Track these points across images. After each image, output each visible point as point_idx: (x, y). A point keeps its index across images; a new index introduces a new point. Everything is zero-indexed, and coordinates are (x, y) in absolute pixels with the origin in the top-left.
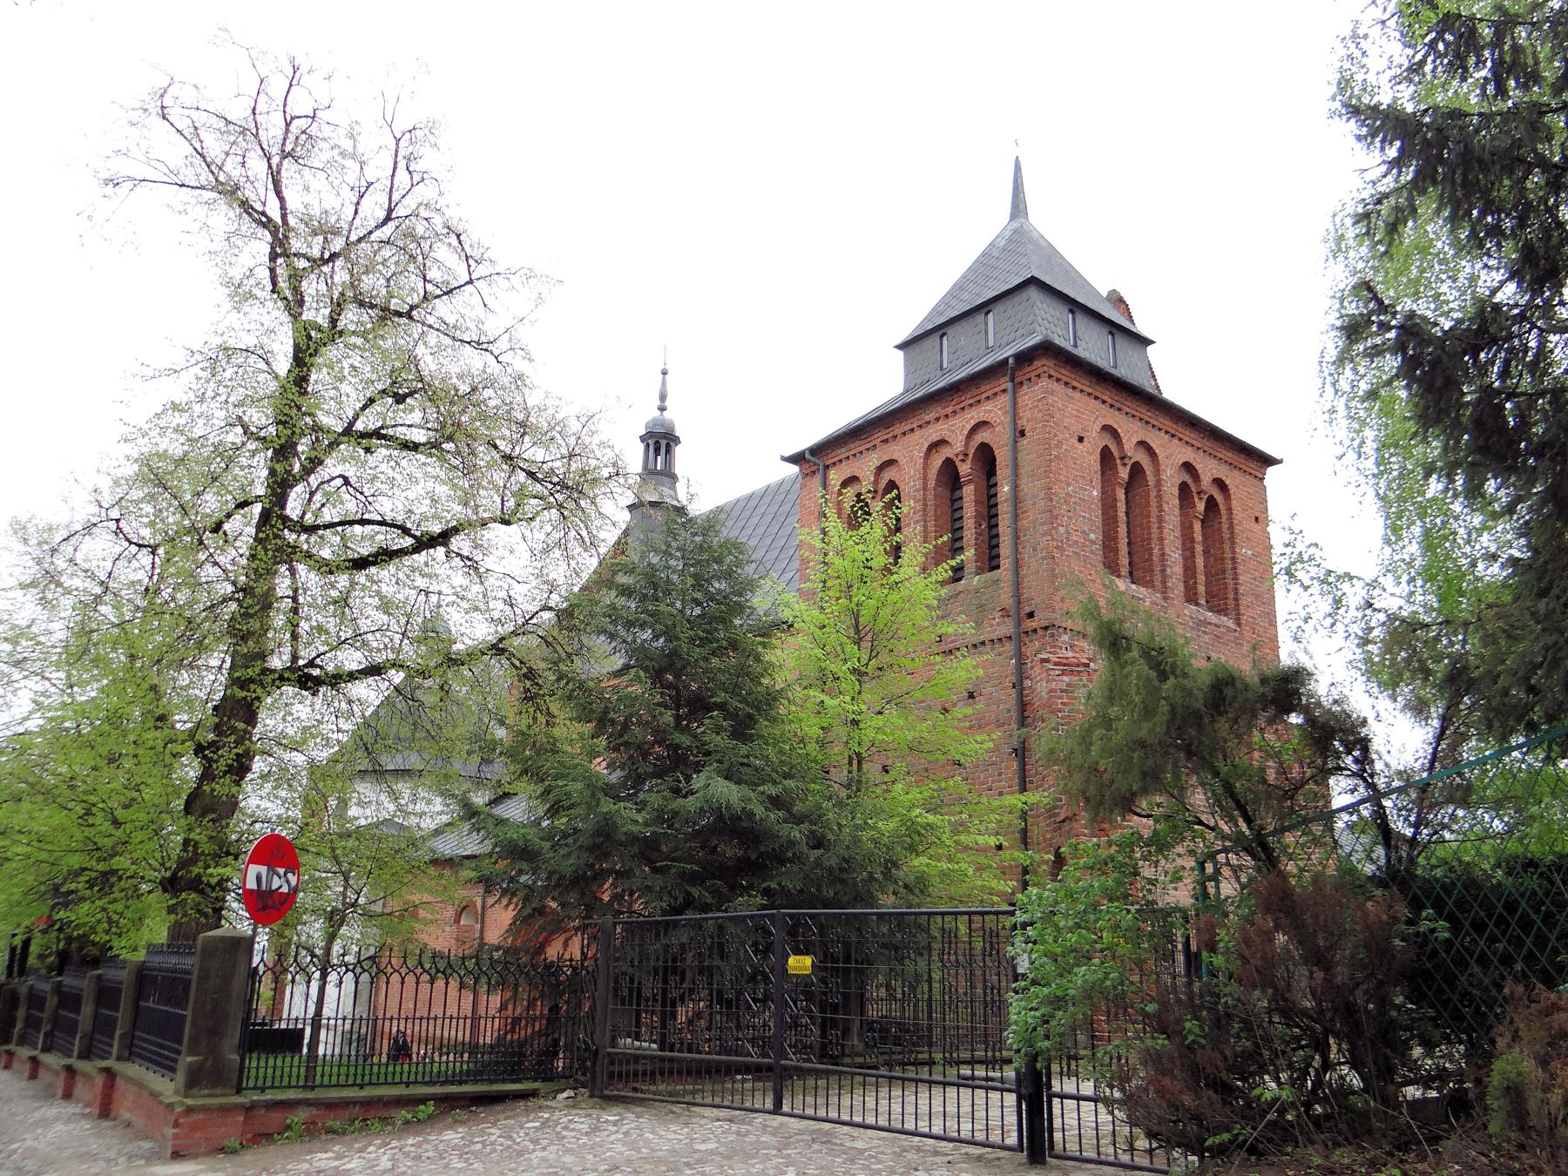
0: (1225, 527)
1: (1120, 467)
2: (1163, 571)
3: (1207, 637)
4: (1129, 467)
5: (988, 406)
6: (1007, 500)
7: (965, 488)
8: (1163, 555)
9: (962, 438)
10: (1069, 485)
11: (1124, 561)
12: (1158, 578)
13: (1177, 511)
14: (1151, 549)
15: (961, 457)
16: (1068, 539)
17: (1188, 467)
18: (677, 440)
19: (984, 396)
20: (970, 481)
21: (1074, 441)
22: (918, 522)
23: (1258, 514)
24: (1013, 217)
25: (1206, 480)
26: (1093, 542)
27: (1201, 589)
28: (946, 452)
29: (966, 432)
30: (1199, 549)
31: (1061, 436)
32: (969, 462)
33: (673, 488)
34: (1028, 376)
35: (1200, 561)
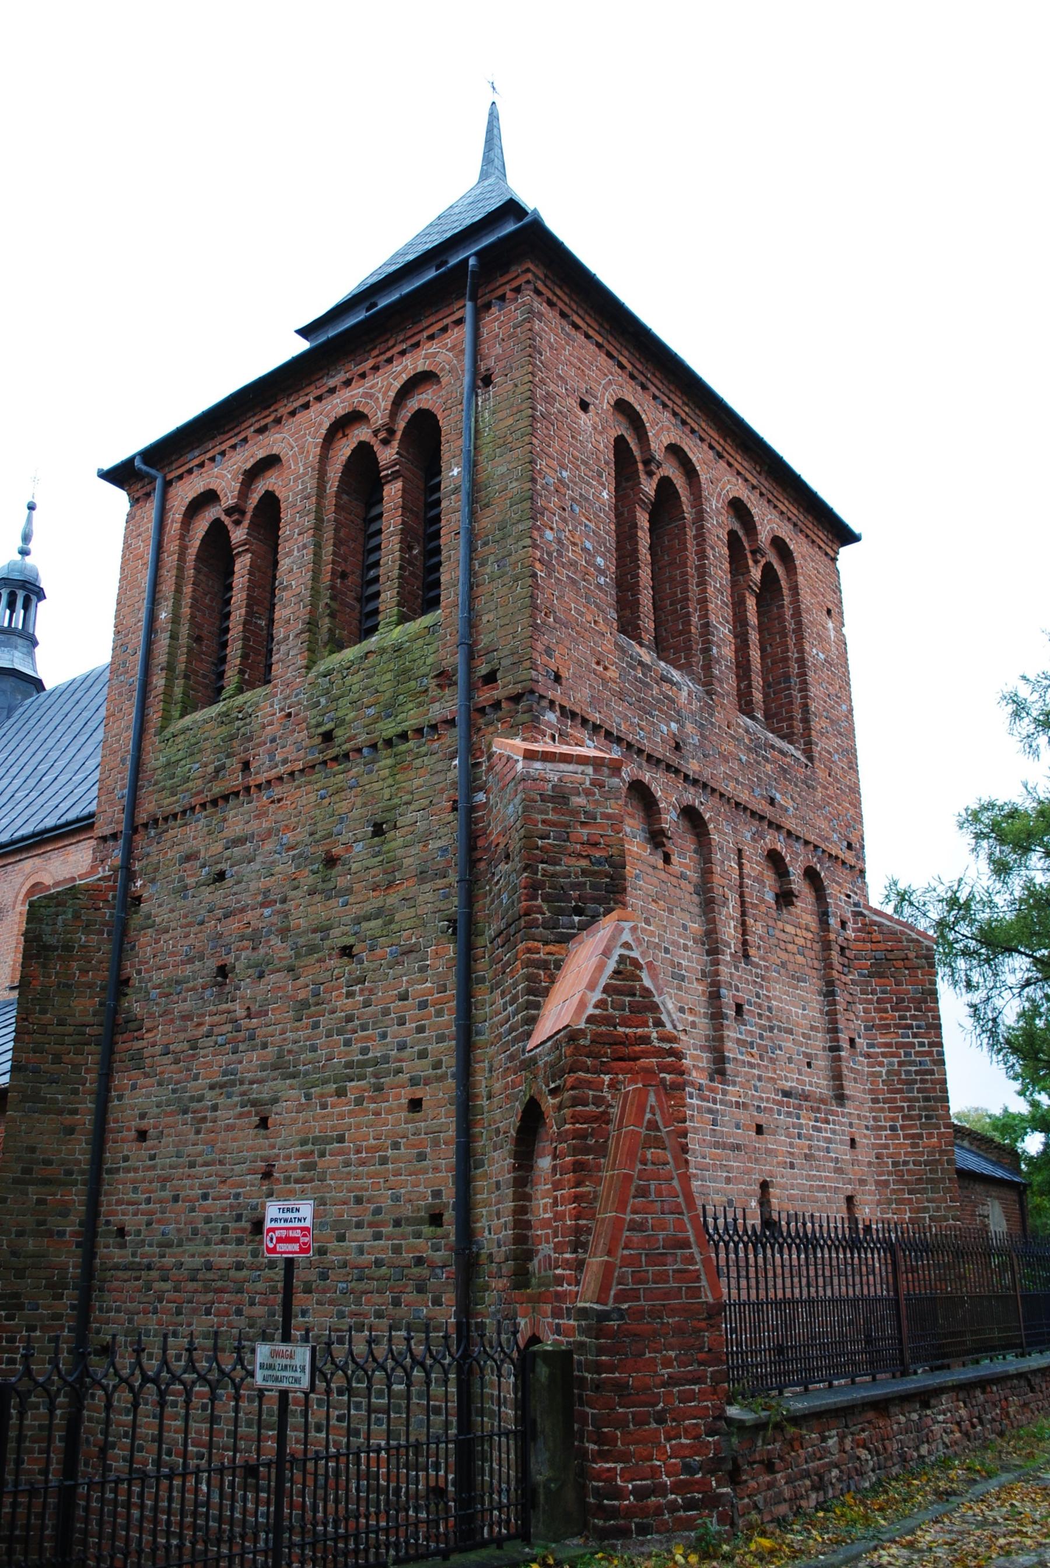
0: (788, 613)
1: (643, 477)
2: (706, 651)
3: (769, 767)
4: (656, 479)
5: (432, 348)
6: (456, 490)
7: (386, 488)
8: (707, 625)
9: (385, 404)
10: (563, 467)
11: (648, 623)
12: (698, 659)
13: (726, 566)
14: (688, 614)
15: (382, 435)
16: (560, 555)
17: (737, 507)
18: (41, 595)
19: (425, 334)
20: (396, 476)
21: (573, 403)
22: (305, 547)
23: (830, 606)
24: (484, 175)
25: (764, 537)
26: (602, 572)
27: (758, 696)
28: (362, 433)
29: (392, 394)
30: (754, 636)
31: (552, 388)
32: (395, 444)
33: (31, 654)
34: (499, 292)
35: (755, 654)
